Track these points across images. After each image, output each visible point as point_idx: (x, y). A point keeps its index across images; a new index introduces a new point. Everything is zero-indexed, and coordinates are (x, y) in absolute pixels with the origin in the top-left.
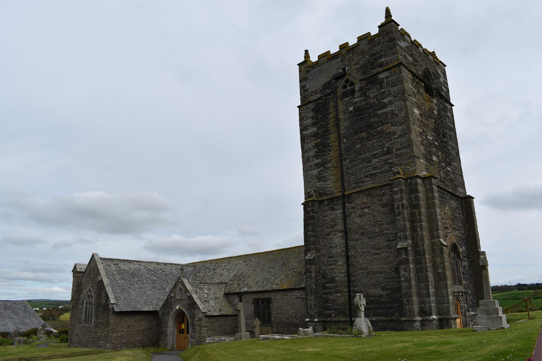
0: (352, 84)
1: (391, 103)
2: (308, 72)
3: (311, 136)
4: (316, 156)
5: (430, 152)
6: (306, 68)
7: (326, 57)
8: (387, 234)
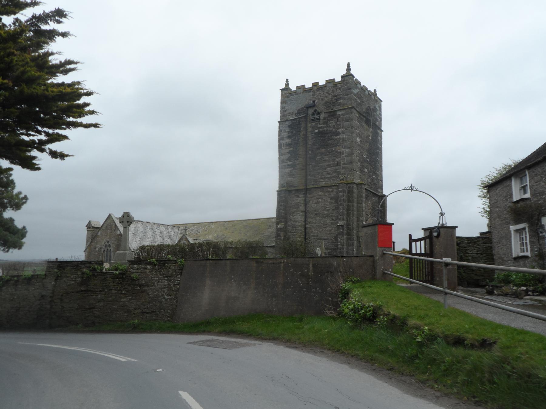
0: (319, 113)
1: (343, 133)
2: (288, 97)
4: (289, 159)
7: (301, 89)
8: (332, 216)
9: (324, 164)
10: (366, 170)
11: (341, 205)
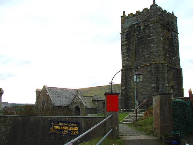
0: (140, 27)
1: (153, 36)
2: (124, 20)
3: (125, 45)
4: (127, 52)
5: (166, 53)
6: (124, 19)
7: (131, 15)
8: (149, 82)
9: (144, 53)
10: (168, 55)
11: (153, 75)
